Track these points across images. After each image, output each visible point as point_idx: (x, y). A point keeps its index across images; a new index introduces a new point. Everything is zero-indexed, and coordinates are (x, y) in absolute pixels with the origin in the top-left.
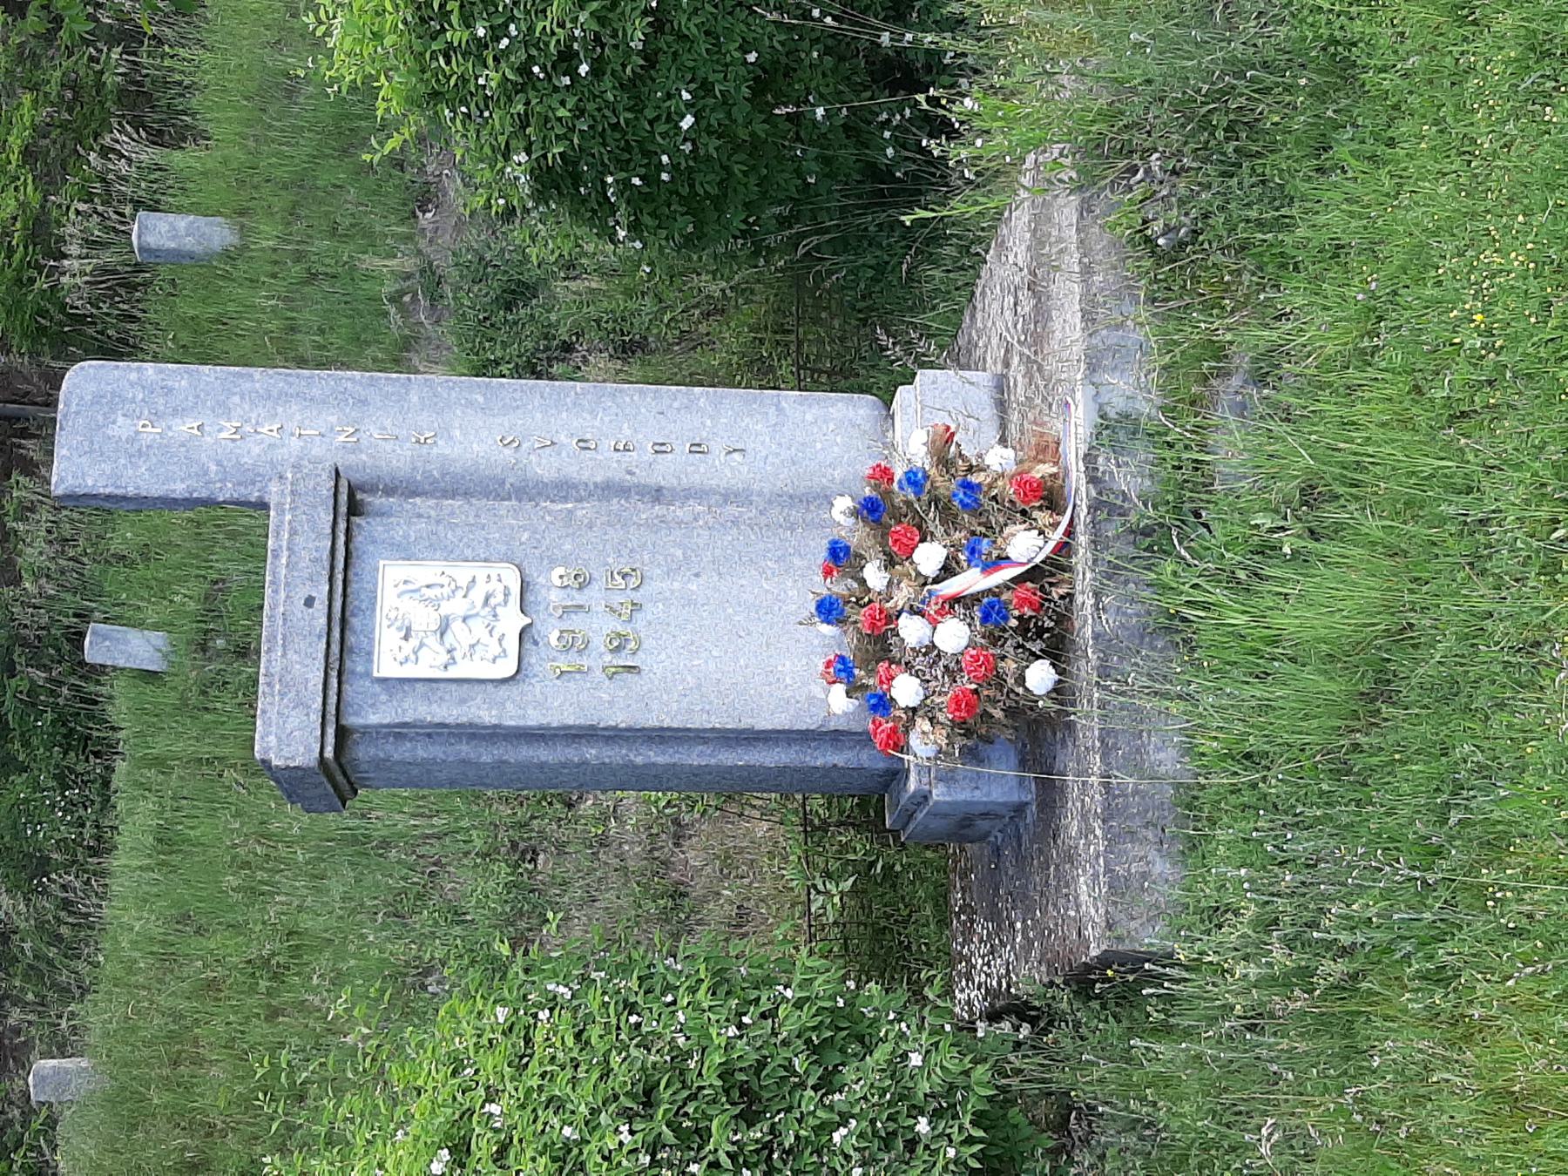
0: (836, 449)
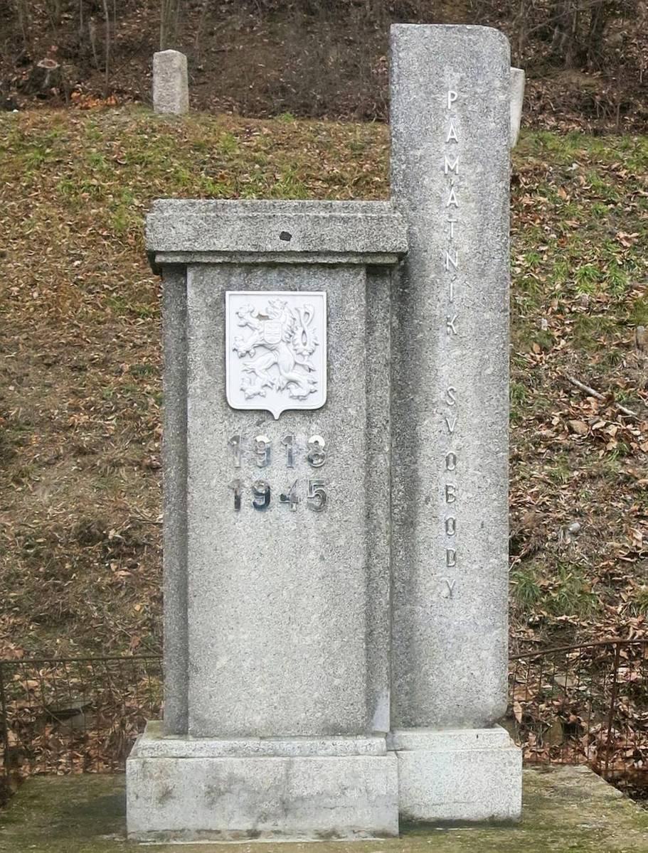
0: (456, 678)
